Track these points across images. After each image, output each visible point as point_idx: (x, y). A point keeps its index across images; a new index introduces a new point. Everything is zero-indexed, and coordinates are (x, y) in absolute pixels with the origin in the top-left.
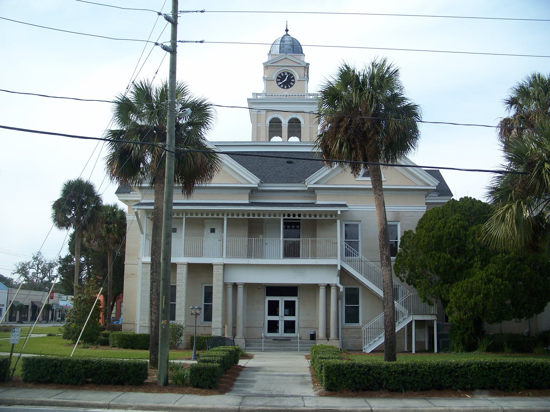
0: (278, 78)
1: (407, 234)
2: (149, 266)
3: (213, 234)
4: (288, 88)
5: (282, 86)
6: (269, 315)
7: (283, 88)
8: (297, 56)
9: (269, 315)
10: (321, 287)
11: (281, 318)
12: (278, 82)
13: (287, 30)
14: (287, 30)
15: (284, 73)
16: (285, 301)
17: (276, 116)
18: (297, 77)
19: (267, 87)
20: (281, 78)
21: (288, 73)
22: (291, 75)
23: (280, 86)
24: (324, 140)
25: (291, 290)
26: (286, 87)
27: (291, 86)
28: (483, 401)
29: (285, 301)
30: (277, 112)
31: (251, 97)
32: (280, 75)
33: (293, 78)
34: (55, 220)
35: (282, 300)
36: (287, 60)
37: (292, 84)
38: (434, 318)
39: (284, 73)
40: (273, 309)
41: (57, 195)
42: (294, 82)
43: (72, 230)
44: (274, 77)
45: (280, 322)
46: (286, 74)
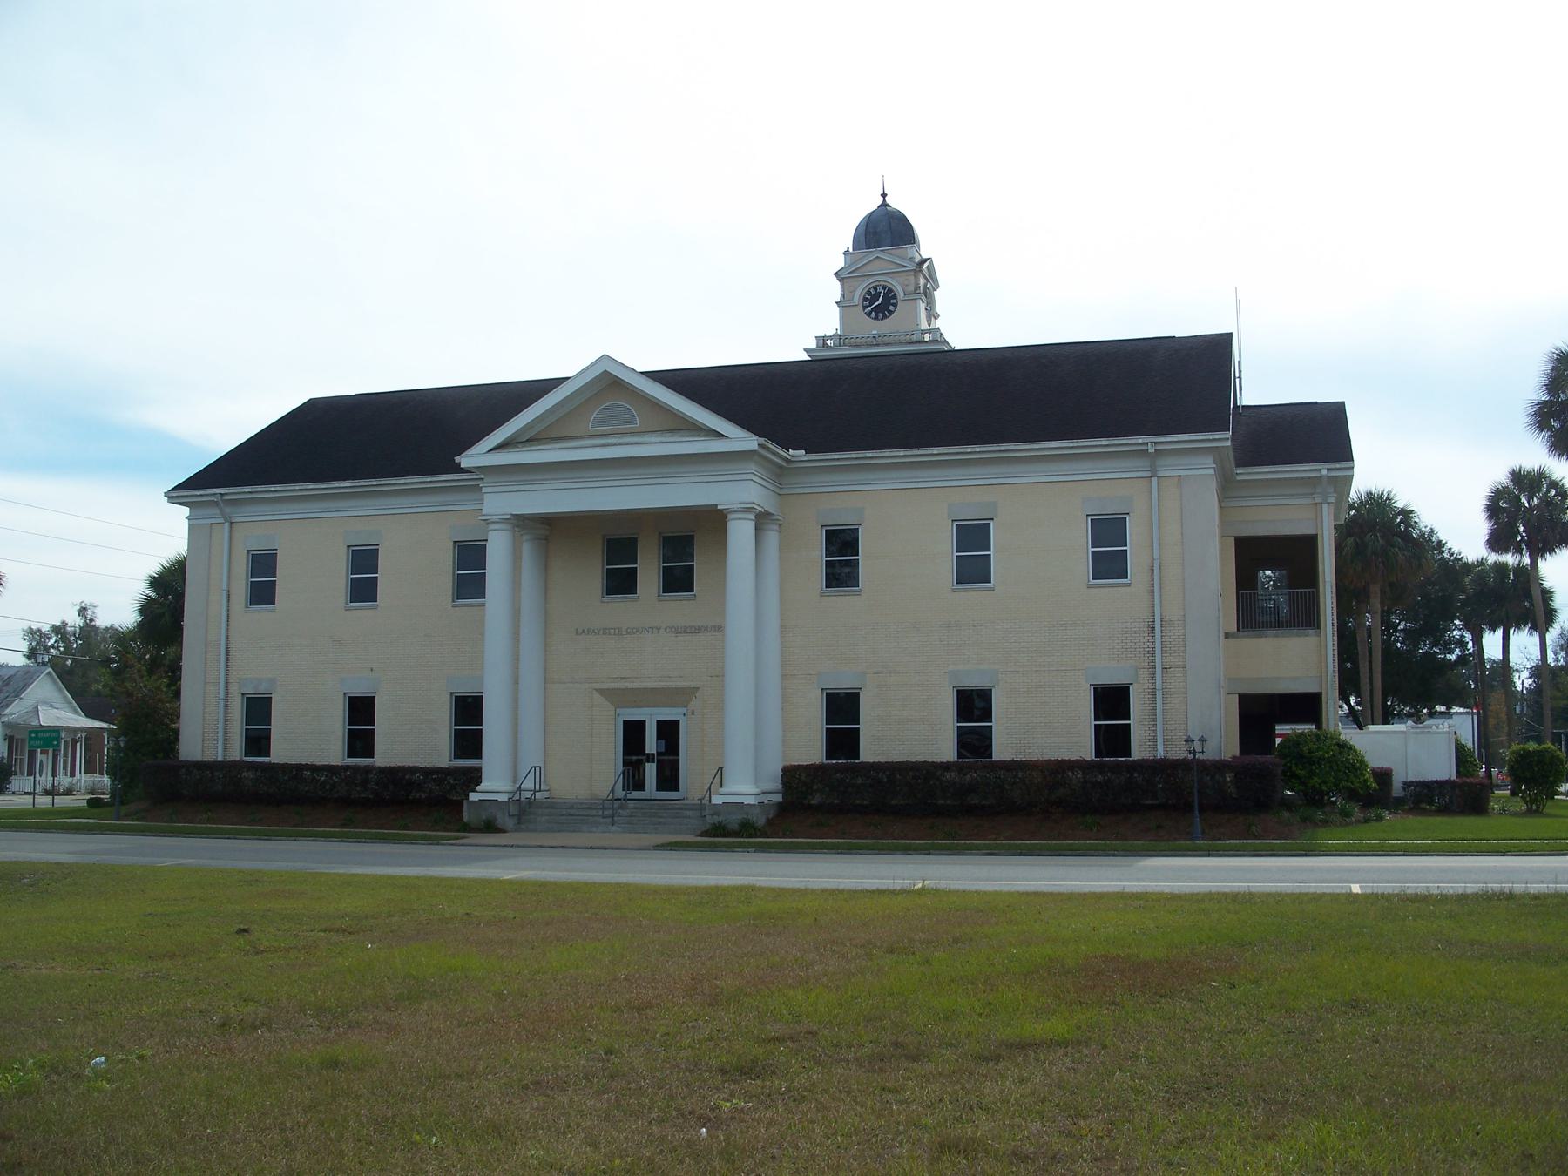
0: (865, 299)
1: (1494, 630)
3: (973, 682)
4: (884, 317)
7: (876, 318)
8: (899, 250)
12: (865, 307)
13: (884, 195)
14: (884, 195)
18: (901, 295)
19: (844, 320)
20: (870, 297)
22: (890, 290)
23: (869, 314)
27: (891, 313)
31: (813, 345)
32: (869, 293)
33: (895, 297)
34: (932, 276)
41: (1557, 603)
42: (895, 305)
44: (857, 299)
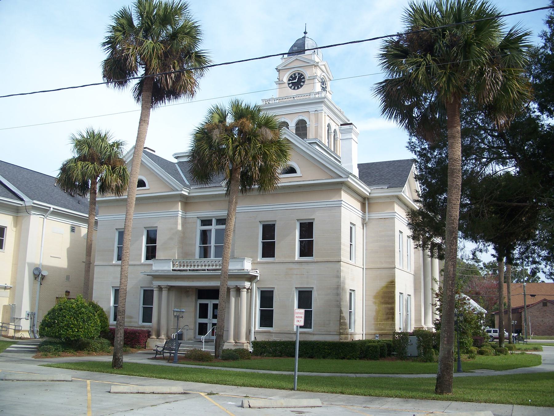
2: (335, 338)
5: (291, 85)
6: (200, 318)
9: (200, 318)
10: (231, 290)
11: (209, 321)
13: (305, 33)
15: (295, 74)
16: (213, 304)
17: (301, 118)
21: (299, 74)
22: (302, 75)
24: (193, 153)
25: (213, 293)
26: (296, 88)
27: (302, 86)
28: (274, 390)
29: (213, 304)
30: (284, 116)
32: (291, 77)
33: (304, 78)
35: (210, 303)
36: (297, 61)
37: (302, 84)
38: (455, 375)
39: (295, 74)
40: (203, 312)
42: (304, 82)
43: (434, 330)
45: (208, 325)
46: (297, 75)
